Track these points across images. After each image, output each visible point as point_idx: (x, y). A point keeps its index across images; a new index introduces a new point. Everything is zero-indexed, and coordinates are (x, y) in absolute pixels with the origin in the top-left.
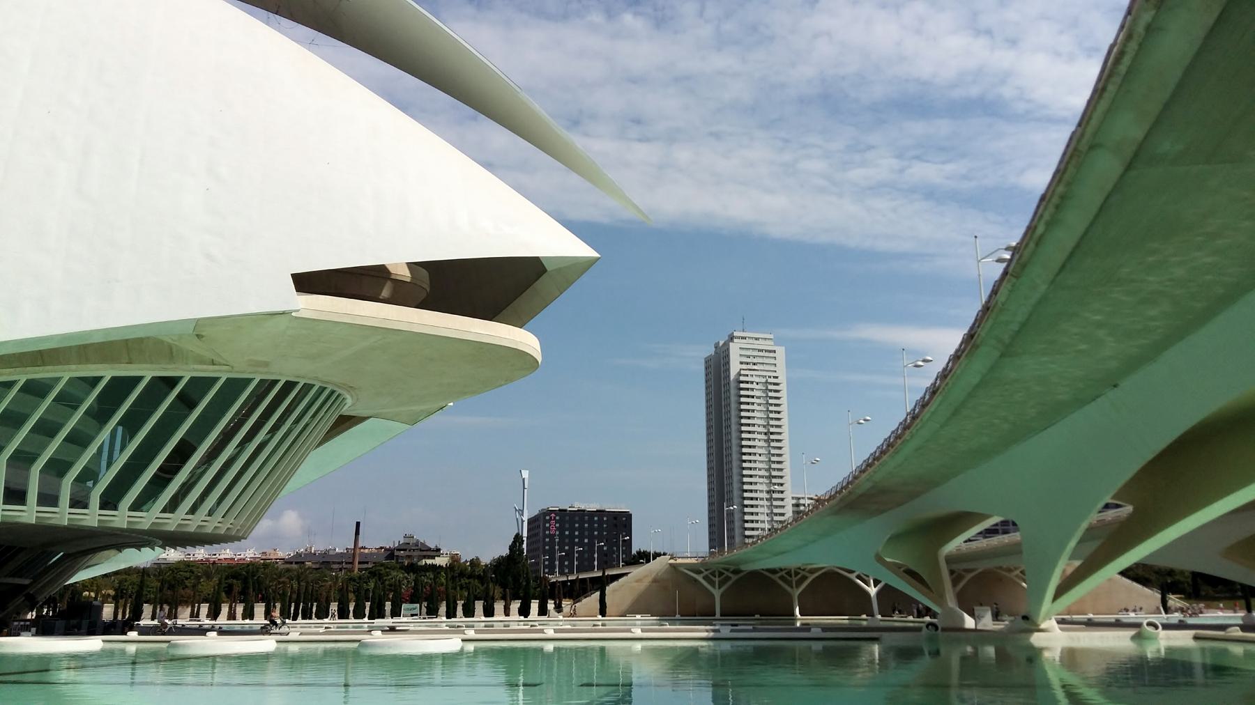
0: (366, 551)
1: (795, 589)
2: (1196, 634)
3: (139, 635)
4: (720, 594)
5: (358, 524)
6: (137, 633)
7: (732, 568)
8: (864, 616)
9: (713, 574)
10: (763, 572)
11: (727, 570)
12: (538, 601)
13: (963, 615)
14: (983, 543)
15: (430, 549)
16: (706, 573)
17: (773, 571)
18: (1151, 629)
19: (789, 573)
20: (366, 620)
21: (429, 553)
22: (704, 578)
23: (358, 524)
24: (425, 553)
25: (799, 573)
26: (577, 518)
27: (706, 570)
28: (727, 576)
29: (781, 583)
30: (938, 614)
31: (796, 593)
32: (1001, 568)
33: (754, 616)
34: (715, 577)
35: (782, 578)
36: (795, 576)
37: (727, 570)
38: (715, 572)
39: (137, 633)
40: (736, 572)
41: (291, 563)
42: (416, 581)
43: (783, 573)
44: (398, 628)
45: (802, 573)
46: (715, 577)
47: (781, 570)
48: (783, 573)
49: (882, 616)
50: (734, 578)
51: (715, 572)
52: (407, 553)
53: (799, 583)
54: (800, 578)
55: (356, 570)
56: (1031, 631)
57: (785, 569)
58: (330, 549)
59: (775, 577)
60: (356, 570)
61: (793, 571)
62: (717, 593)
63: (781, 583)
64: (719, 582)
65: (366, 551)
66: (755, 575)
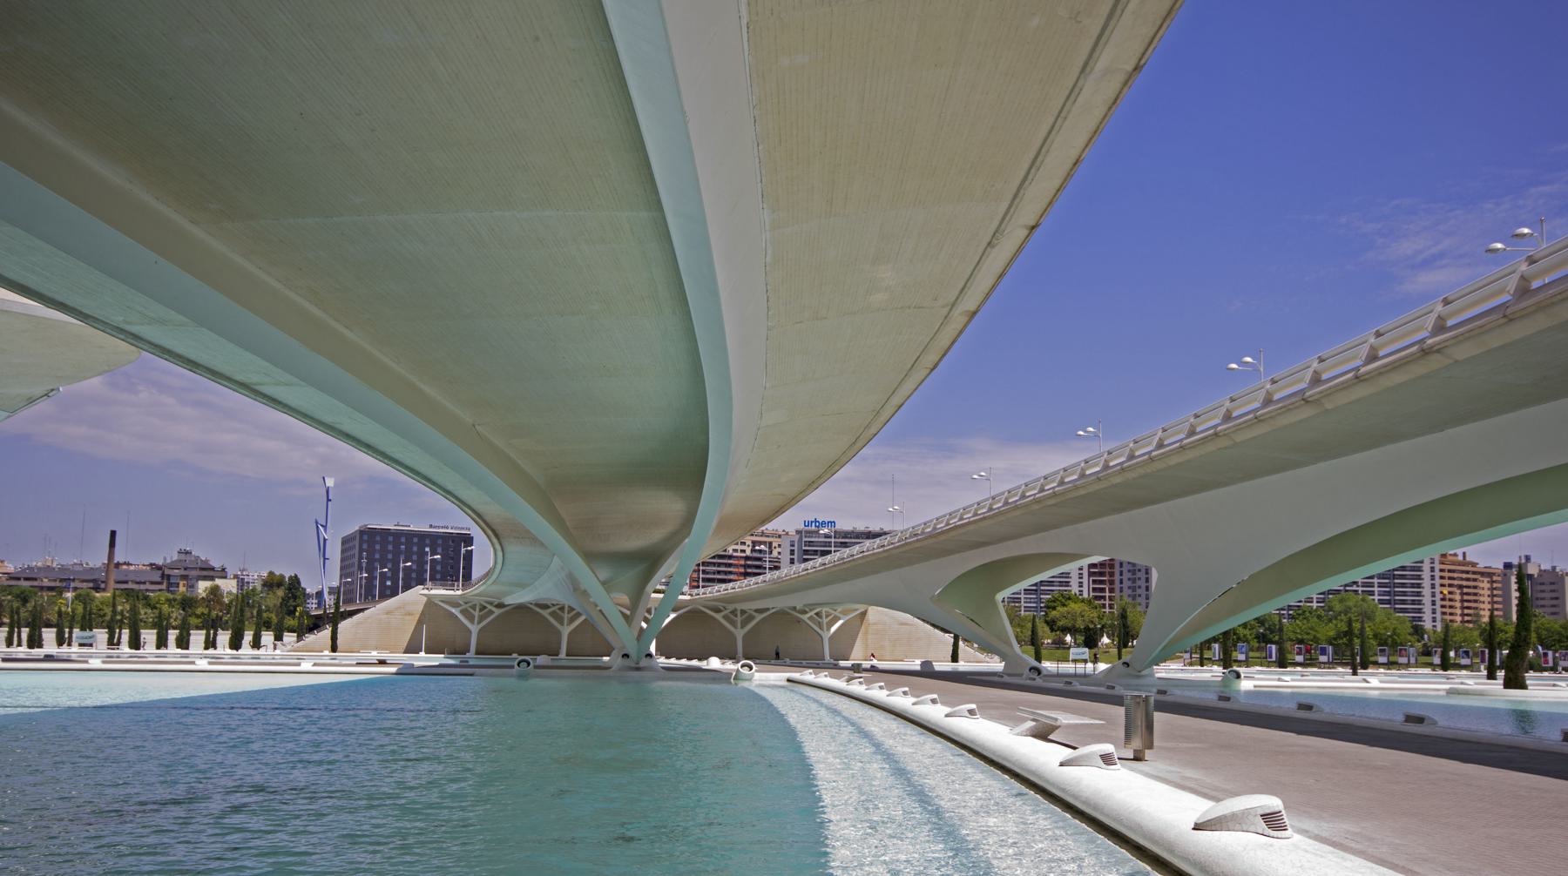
0: (132, 568)
1: (826, 632)
4: (478, 630)
5: (113, 534)
7: (496, 602)
9: (474, 607)
10: (531, 606)
11: (491, 603)
12: (155, 631)
15: (213, 569)
16: (553, 609)
17: (545, 607)
19: (562, 609)
20: (422, 654)
21: (211, 573)
23: (113, 534)
24: (205, 573)
26: (378, 538)
27: (466, 603)
29: (551, 620)
31: (566, 631)
32: (794, 608)
33: (511, 655)
34: (475, 610)
35: (553, 614)
36: (568, 613)
37: (491, 603)
38: (476, 605)
40: (500, 606)
41: (19, 579)
42: (266, 612)
44: (388, 662)
46: (475, 610)
47: (553, 605)
50: (497, 612)
51: (476, 605)
52: (183, 572)
53: (571, 620)
54: (575, 615)
58: (75, 564)
59: (545, 613)
60: (808, 615)
62: (474, 629)
63: (551, 620)
65: (132, 568)
66: (521, 608)
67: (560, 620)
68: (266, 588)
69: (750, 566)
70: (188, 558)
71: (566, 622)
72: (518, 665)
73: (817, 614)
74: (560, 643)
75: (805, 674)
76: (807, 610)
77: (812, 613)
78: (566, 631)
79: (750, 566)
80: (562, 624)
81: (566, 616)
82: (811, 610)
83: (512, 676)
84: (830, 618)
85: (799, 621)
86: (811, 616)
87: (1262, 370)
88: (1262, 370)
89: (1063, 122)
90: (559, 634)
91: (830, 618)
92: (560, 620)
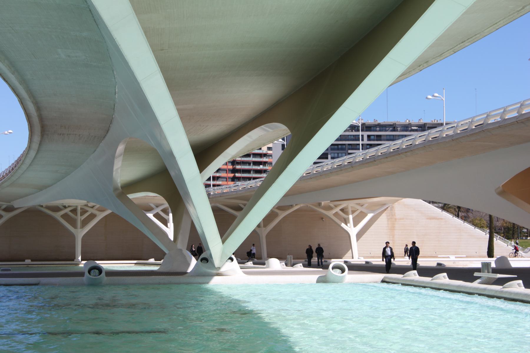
2: (385, 277)
3: (155, 260)
6: (154, 259)
8: (152, 260)
13: (192, 257)
14: (328, 164)
17: (56, 209)
18: (337, 272)
19: (74, 211)
22: (154, 216)
25: (87, 211)
28: (361, 212)
30: (166, 254)
31: (80, 233)
33: (24, 261)
35: (65, 216)
36: (81, 215)
39: (154, 259)
43: (67, 210)
45: (91, 211)
47: (65, 207)
48: (67, 210)
49: (155, 260)
53: (85, 223)
55: (334, 211)
56: (212, 275)
57: (69, 206)
59: (58, 216)
60: (334, 211)
61: (79, 208)
64: (353, 219)
67: (73, 223)
68: (512, 225)
69: (239, 171)
70: (492, 229)
71: (79, 224)
72: (89, 272)
73: (342, 210)
74: (74, 247)
75: (409, 276)
76: (332, 205)
77: (337, 210)
78: (80, 233)
79: (239, 171)
80: (75, 226)
81: (80, 218)
82: (336, 206)
83: (82, 285)
84: (356, 214)
85: (322, 218)
86: (336, 213)
87: (444, 99)
88: (444, 99)
89: (340, 171)
90: (72, 237)
91: (356, 214)
92: (73, 223)
